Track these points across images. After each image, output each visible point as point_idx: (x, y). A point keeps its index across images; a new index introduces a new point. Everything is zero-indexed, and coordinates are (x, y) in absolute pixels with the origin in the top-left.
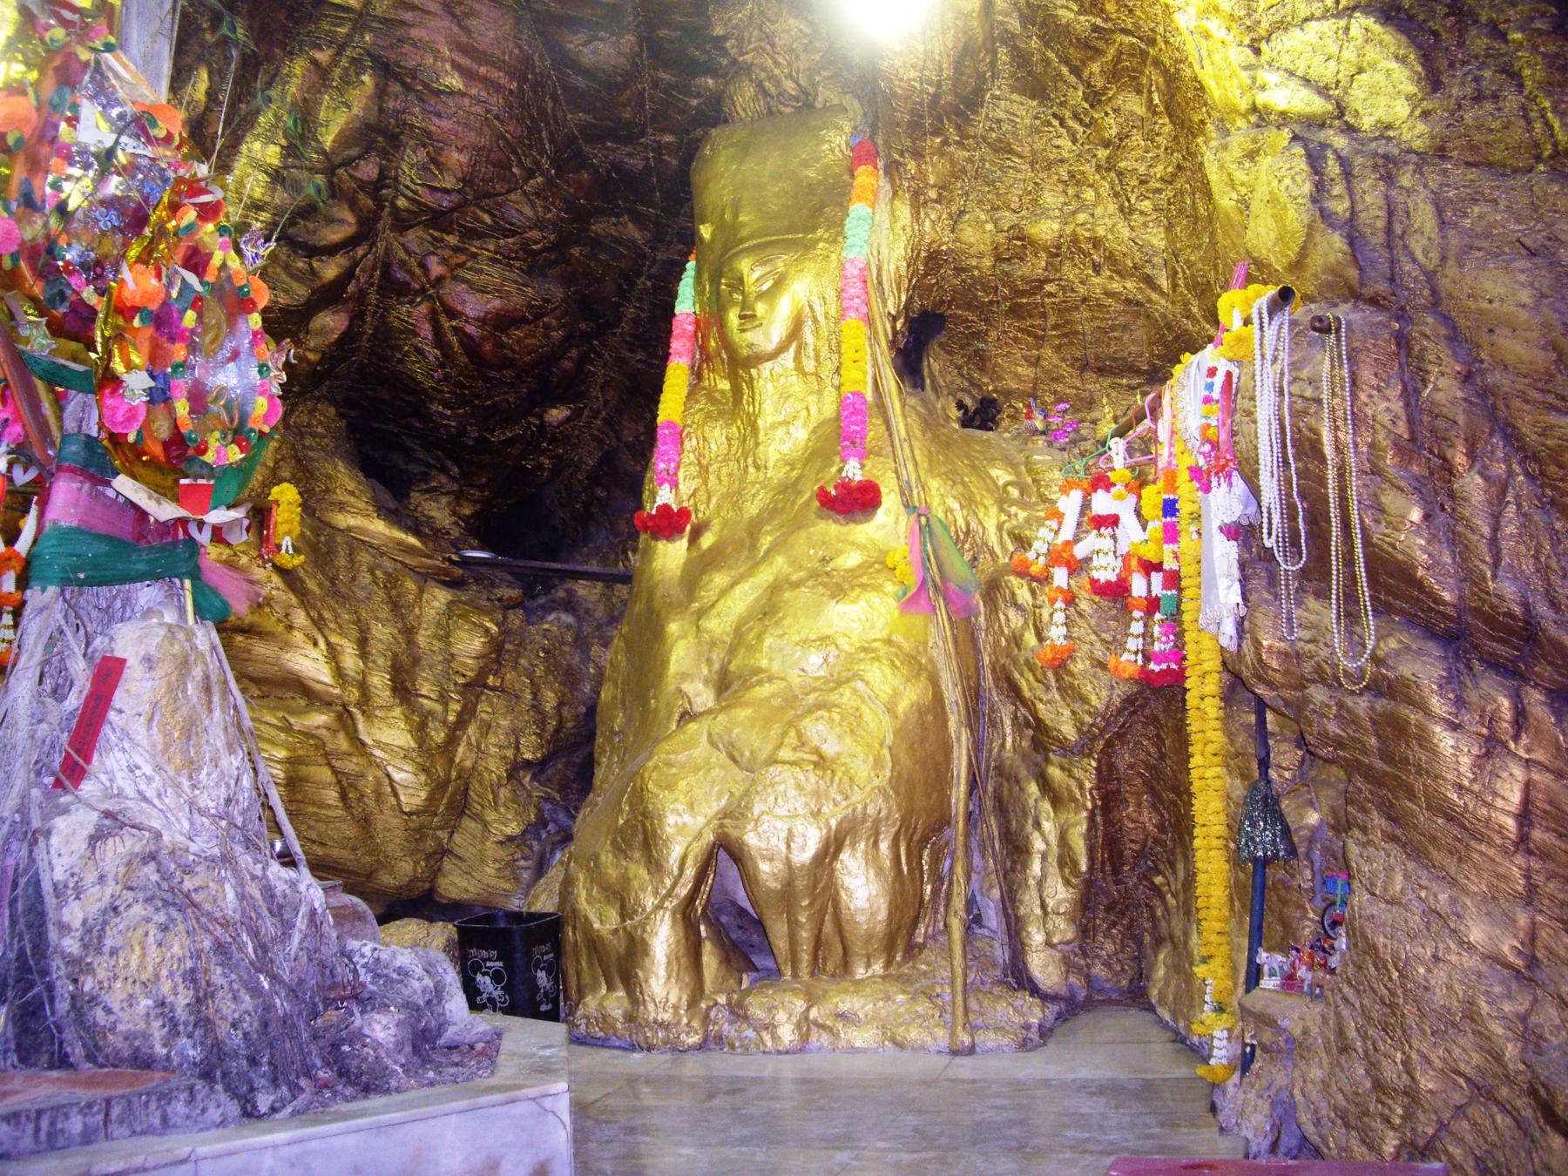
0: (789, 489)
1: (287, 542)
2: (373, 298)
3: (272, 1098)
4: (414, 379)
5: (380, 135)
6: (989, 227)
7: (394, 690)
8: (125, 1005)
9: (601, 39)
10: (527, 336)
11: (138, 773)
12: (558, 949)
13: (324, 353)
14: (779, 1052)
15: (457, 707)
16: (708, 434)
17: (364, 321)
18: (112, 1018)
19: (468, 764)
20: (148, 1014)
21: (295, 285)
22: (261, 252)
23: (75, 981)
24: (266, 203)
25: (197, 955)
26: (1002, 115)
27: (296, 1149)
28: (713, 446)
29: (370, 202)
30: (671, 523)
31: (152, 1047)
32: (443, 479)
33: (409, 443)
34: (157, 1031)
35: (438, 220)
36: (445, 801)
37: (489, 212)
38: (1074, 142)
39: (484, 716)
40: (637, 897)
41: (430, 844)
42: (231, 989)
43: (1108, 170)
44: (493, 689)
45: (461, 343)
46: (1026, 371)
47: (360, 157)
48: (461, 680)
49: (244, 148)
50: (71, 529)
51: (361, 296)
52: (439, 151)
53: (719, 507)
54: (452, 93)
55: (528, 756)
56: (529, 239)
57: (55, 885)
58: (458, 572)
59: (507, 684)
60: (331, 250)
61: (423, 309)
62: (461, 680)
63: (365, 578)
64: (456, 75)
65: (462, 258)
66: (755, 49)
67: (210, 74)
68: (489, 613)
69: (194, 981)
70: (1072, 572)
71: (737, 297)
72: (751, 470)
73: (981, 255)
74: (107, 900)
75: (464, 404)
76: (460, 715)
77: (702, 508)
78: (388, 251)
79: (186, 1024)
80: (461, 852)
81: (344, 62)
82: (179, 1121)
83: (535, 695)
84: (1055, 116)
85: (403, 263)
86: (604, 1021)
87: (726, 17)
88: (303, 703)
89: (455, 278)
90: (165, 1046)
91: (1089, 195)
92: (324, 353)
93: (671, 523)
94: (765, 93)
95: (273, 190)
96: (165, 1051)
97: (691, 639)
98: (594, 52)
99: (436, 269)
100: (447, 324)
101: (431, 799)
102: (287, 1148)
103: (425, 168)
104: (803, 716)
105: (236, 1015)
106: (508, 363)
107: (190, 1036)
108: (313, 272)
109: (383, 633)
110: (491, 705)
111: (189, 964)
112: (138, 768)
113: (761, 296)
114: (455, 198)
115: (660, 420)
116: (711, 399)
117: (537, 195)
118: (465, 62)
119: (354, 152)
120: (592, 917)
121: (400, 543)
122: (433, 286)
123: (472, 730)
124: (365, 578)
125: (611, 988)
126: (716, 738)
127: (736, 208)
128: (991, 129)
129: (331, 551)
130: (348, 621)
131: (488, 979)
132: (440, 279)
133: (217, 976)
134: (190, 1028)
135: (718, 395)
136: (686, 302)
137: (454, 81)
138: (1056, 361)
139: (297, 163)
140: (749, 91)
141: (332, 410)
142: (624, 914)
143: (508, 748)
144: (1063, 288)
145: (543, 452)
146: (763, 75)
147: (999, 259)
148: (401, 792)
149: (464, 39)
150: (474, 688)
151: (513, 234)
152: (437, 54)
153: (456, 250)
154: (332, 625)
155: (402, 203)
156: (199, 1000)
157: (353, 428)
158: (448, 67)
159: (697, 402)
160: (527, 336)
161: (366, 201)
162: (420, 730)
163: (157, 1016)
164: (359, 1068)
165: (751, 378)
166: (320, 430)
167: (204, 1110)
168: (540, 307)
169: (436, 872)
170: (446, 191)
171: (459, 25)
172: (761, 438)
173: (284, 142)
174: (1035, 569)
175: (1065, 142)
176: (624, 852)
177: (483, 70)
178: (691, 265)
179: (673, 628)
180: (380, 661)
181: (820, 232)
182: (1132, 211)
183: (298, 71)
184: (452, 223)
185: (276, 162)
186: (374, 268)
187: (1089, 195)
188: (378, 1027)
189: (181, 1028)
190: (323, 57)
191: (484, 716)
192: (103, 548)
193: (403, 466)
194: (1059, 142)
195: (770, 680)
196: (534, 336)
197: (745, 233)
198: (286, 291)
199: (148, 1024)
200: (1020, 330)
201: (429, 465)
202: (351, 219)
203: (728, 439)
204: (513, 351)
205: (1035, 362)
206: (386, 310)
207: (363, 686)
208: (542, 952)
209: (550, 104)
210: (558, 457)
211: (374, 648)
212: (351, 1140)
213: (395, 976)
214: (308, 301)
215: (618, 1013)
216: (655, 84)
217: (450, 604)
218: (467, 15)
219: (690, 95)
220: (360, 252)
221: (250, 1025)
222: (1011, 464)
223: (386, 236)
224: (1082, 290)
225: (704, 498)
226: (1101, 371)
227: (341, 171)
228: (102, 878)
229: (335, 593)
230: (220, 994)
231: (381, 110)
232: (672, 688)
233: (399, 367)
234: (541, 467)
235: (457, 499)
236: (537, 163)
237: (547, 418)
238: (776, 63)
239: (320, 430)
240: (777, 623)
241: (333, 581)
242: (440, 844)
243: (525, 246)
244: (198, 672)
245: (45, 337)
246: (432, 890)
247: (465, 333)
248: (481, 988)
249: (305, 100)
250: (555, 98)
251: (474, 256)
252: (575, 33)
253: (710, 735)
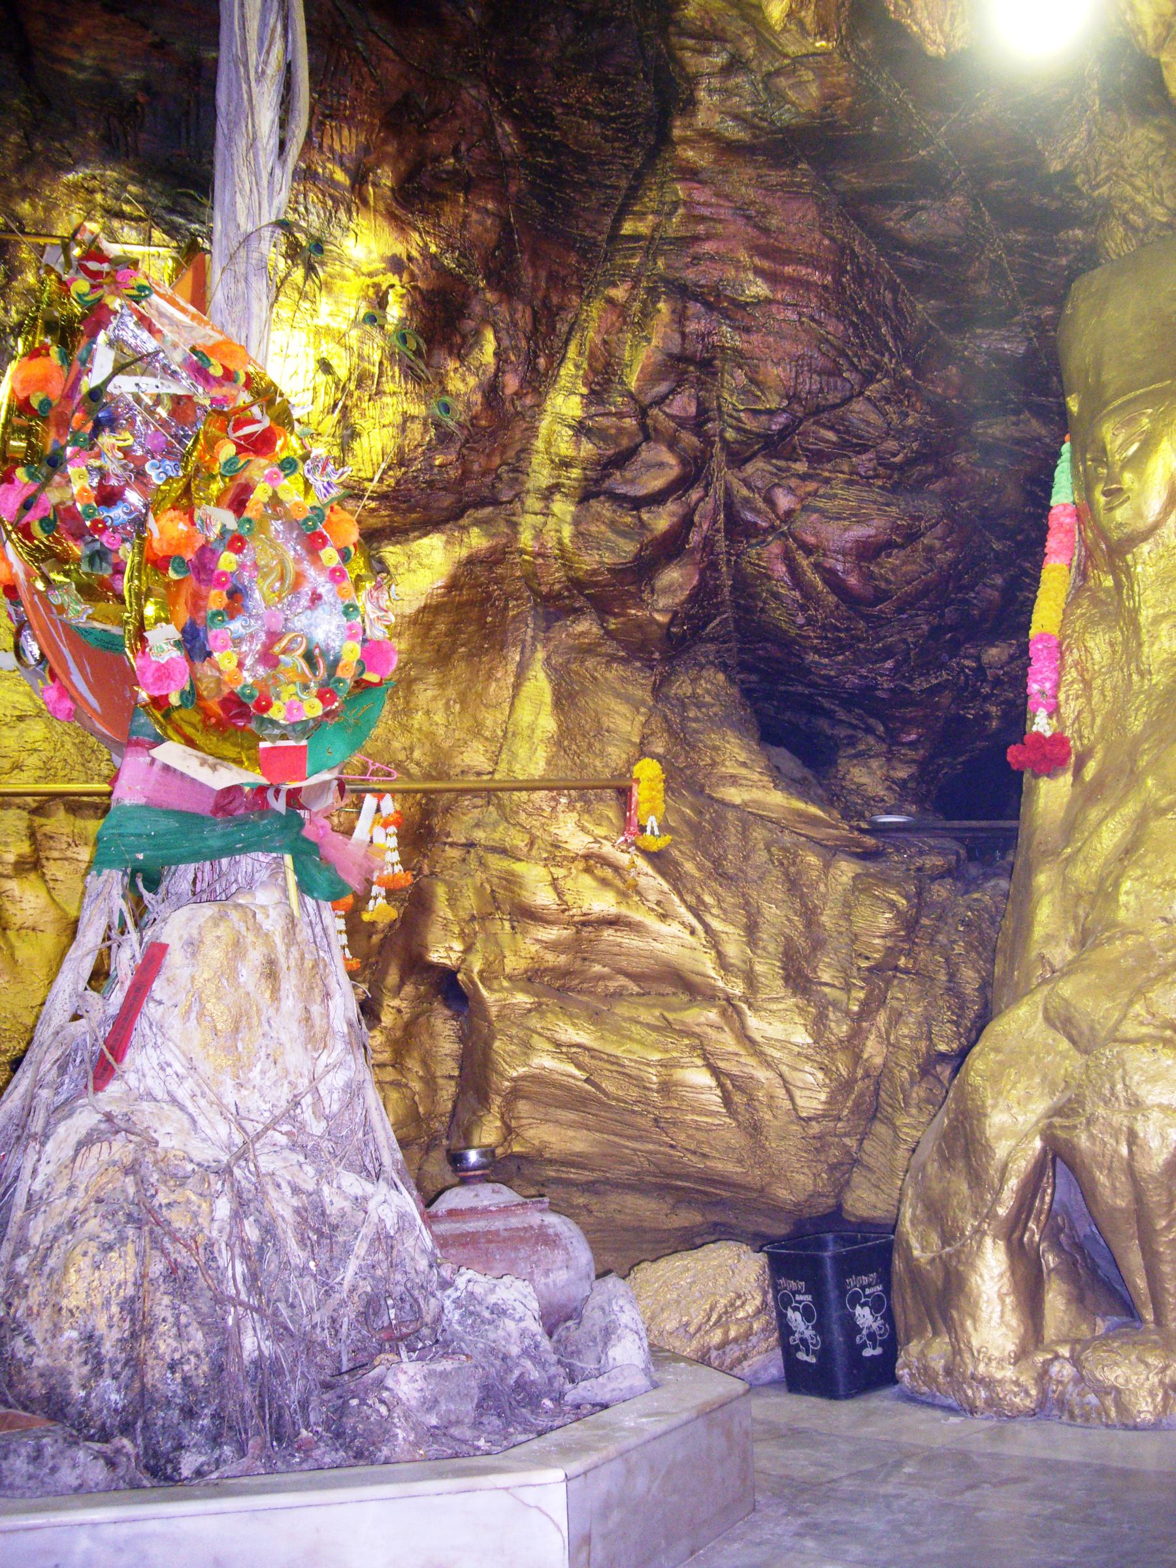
1: (652, 822)
2: (722, 544)
3: (203, 1459)
4: (780, 628)
5: (691, 365)
7: (787, 979)
8: (49, 1335)
9: (922, 208)
10: (904, 563)
11: (169, 1070)
12: (886, 1279)
13: (675, 613)
14: (1126, 1427)
15: (861, 995)
16: (1090, 644)
17: (718, 571)
18: (32, 1349)
19: (878, 1061)
20: (70, 1348)
21: (621, 542)
22: (335, 479)
23: (9, 1305)
24: (573, 458)
25: (142, 1279)
27: (125, 1530)
28: (1097, 657)
29: (695, 439)
31: (68, 1386)
32: (871, 740)
33: (827, 705)
34: (77, 1369)
35: (774, 445)
36: (849, 1104)
37: (831, 428)
39: (895, 1004)
40: (955, 1220)
41: (835, 1154)
42: (177, 1324)
44: (906, 971)
45: (825, 582)
47: (672, 392)
48: (864, 964)
49: (548, 406)
50: (137, 807)
51: (708, 543)
52: (755, 370)
53: (1103, 729)
54: (760, 302)
55: (942, 1048)
56: (885, 452)
57: (30, 1196)
58: (870, 841)
60: (657, 499)
61: (775, 548)
62: (864, 964)
63: (761, 857)
64: (759, 281)
65: (811, 486)
66: (1108, 179)
67: (496, 332)
68: (897, 885)
69: (132, 1311)
71: (1103, 471)
72: (1135, 677)
74: (68, 1214)
75: (841, 649)
76: (864, 1004)
77: (1086, 733)
78: (728, 492)
79: (113, 1362)
80: (871, 1162)
81: (643, 295)
82: (18, 1481)
83: (952, 977)
85: (746, 500)
86: (926, 1374)
87: (1059, 147)
88: (685, 998)
89: (804, 509)
90: (84, 1387)
92: (675, 613)
93: (1053, 755)
94: (1134, 229)
95: (578, 444)
96: (83, 1393)
97: (1057, 892)
98: (920, 225)
99: (784, 501)
100: (804, 562)
101: (831, 1101)
102: (112, 1527)
103: (745, 392)
104: (1152, 981)
105: (177, 1356)
106: (881, 596)
107: (115, 1377)
108: (643, 524)
109: (775, 913)
110: (902, 990)
111: (130, 1291)
112: (169, 1065)
113: (1127, 464)
114: (782, 419)
115: (1033, 633)
116: (1095, 601)
117: (888, 401)
118: (766, 264)
119: (663, 388)
120: (914, 1243)
121: (800, 814)
122: (785, 522)
123: (882, 1018)
124: (761, 857)
125: (936, 1333)
126: (1052, 1014)
127: (1098, 365)
129: (718, 824)
130: (735, 905)
131: (798, 1315)
132: (789, 513)
133: (162, 1305)
134: (118, 1368)
135: (1102, 595)
136: (1063, 493)
137: (758, 289)
139: (601, 410)
140: (1120, 232)
141: (721, 677)
142: (946, 1240)
143: (920, 1039)
145: (987, 698)
146: (1126, 206)
148: (797, 1093)
149: (763, 241)
150: (882, 972)
151: (865, 449)
152: (738, 266)
153: (804, 477)
154: (715, 911)
155: (730, 434)
156: (134, 1335)
157: (747, 693)
158: (751, 276)
159: (1079, 606)
160: (904, 563)
161: (689, 439)
162: (818, 1025)
163: (80, 1351)
164: (354, 1428)
165: (1128, 566)
166: (708, 699)
167: (54, 1470)
168: (910, 527)
169: (842, 1187)
170: (770, 412)
171: (756, 226)
172: (1145, 637)
173: (584, 391)
176: (947, 1160)
177: (788, 270)
178: (1066, 448)
179: (1042, 879)
180: (771, 948)
183: (595, 314)
184: (794, 448)
186: (716, 513)
188: (403, 1378)
189: (106, 1366)
190: (619, 293)
191: (895, 1004)
192: (173, 824)
193: (829, 732)
195: (1124, 935)
196: (914, 562)
197: (1110, 392)
198: (612, 550)
199: (68, 1358)
201: (854, 727)
202: (670, 459)
203: (1112, 644)
204: (888, 582)
206: (738, 556)
207: (750, 979)
208: (866, 1284)
209: (888, 296)
210: (1007, 702)
211: (765, 934)
212: (211, 1523)
213: (487, 1314)
214: (638, 557)
215: (939, 1365)
216: (1009, 248)
217: (856, 877)
218: (764, 215)
219: (1056, 253)
220: (695, 495)
221: (199, 1370)
223: (724, 476)
225: (1088, 720)
227: (655, 411)
228: (71, 1190)
229: (719, 873)
230: (163, 1328)
231: (684, 336)
232: (1033, 954)
234: (987, 716)
235: (889, 760)
236: (877, 365)
237: (985, 659)
238: (1137, 190)
239: (708, 699)
240: (1136, 863)
241: (717, 863)
242: (848, 1152)
243: (881, 461)
244: (255, 956)
245: (78, 602)
246: (839, 1207)
247: (824, 568)
248: (792, 1325)
249: (605, 342)
250: (894, 289)
251: (827, 481)
252: (892, 207)
253: (1046, 1010)
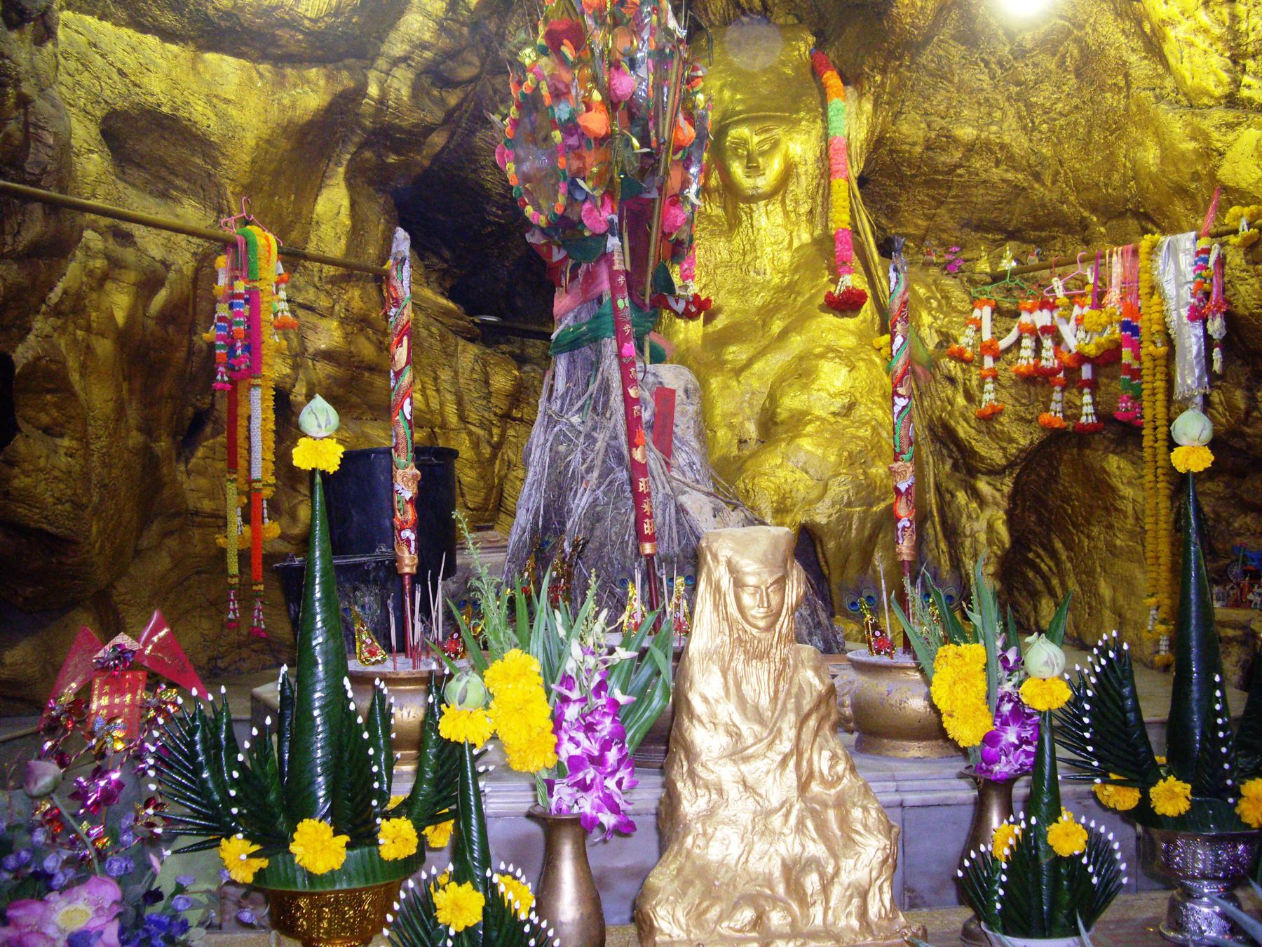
0: (790, 289)
6: (923, 125)
26: (941, 52)
30: (700, 308)
38: (993, 78)
43: (1017, 101)
46: (923, 223)
59: (526, 417)
70: (996, 359)
73: (914, 144)
84: (983, 60)
91: (998, 114)
95: (439, 36)
108: (442, 99)
121: (442, 307)
128: (932, 61)
138: (947, 217)
144: (970, 174)
147: (928, 148)
174: (968, 354)
175: (985, 77)
181: (802, 114)
182: (1034, 129)
185: (441, 14)
187: (998, 114)
194: (981, 77)
198: (431, 112)
200: (928, 195)
205: (930, 218)
222: (928, 287)
224: (984, 176)
226: (978, 228)
233: (473, 176)
